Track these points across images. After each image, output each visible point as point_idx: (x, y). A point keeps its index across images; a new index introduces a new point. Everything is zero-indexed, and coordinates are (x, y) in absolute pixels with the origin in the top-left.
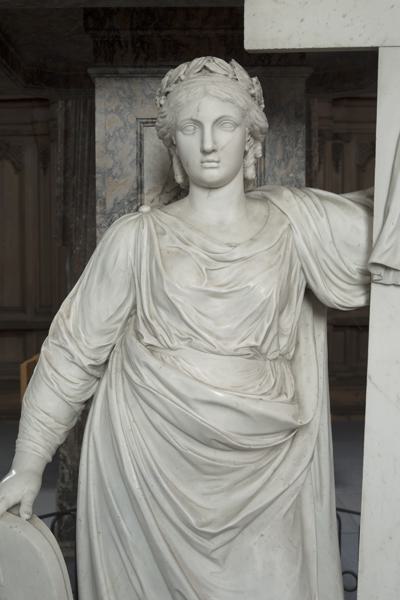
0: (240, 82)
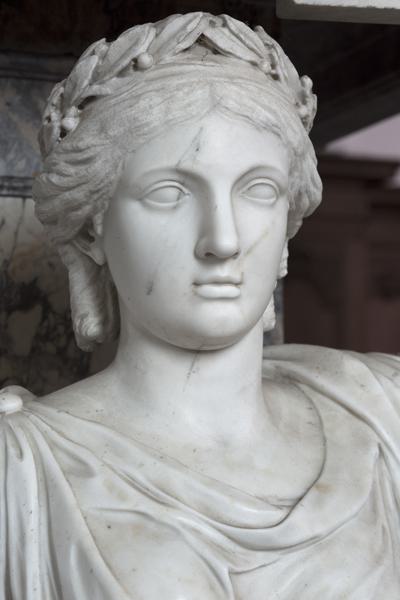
0: (282, 84)
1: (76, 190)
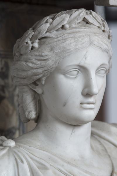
1: (38, 69)
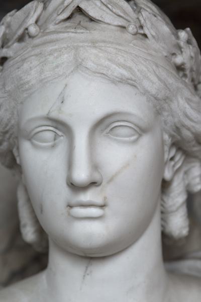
0: (151, 42)
